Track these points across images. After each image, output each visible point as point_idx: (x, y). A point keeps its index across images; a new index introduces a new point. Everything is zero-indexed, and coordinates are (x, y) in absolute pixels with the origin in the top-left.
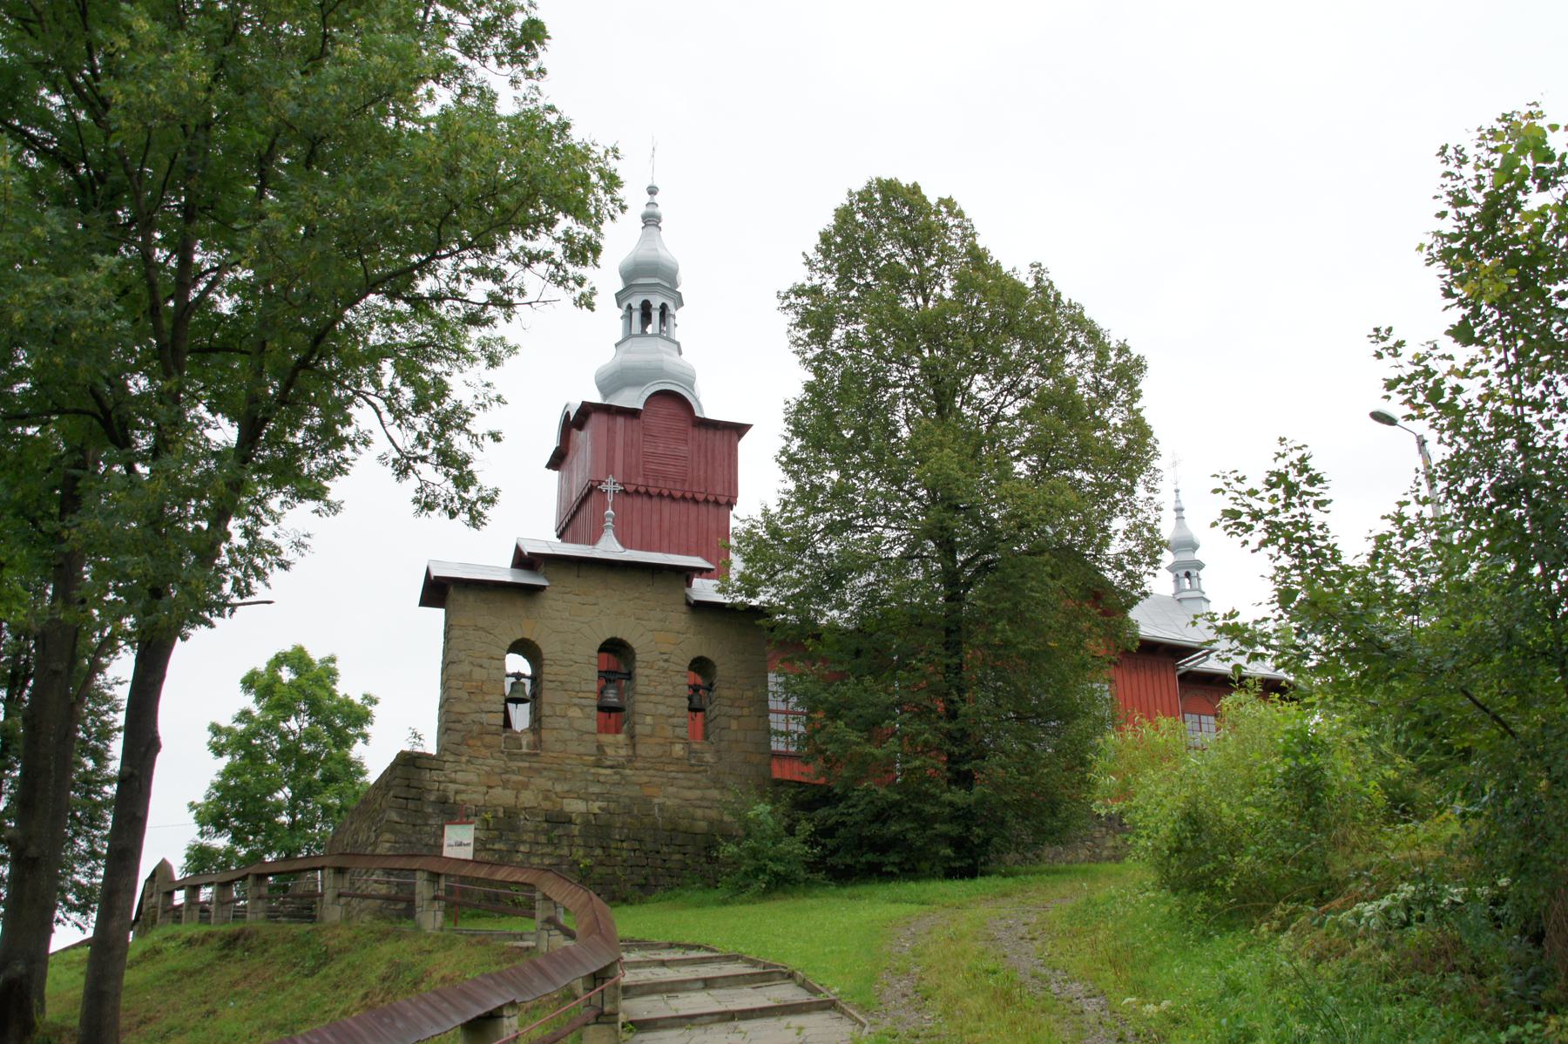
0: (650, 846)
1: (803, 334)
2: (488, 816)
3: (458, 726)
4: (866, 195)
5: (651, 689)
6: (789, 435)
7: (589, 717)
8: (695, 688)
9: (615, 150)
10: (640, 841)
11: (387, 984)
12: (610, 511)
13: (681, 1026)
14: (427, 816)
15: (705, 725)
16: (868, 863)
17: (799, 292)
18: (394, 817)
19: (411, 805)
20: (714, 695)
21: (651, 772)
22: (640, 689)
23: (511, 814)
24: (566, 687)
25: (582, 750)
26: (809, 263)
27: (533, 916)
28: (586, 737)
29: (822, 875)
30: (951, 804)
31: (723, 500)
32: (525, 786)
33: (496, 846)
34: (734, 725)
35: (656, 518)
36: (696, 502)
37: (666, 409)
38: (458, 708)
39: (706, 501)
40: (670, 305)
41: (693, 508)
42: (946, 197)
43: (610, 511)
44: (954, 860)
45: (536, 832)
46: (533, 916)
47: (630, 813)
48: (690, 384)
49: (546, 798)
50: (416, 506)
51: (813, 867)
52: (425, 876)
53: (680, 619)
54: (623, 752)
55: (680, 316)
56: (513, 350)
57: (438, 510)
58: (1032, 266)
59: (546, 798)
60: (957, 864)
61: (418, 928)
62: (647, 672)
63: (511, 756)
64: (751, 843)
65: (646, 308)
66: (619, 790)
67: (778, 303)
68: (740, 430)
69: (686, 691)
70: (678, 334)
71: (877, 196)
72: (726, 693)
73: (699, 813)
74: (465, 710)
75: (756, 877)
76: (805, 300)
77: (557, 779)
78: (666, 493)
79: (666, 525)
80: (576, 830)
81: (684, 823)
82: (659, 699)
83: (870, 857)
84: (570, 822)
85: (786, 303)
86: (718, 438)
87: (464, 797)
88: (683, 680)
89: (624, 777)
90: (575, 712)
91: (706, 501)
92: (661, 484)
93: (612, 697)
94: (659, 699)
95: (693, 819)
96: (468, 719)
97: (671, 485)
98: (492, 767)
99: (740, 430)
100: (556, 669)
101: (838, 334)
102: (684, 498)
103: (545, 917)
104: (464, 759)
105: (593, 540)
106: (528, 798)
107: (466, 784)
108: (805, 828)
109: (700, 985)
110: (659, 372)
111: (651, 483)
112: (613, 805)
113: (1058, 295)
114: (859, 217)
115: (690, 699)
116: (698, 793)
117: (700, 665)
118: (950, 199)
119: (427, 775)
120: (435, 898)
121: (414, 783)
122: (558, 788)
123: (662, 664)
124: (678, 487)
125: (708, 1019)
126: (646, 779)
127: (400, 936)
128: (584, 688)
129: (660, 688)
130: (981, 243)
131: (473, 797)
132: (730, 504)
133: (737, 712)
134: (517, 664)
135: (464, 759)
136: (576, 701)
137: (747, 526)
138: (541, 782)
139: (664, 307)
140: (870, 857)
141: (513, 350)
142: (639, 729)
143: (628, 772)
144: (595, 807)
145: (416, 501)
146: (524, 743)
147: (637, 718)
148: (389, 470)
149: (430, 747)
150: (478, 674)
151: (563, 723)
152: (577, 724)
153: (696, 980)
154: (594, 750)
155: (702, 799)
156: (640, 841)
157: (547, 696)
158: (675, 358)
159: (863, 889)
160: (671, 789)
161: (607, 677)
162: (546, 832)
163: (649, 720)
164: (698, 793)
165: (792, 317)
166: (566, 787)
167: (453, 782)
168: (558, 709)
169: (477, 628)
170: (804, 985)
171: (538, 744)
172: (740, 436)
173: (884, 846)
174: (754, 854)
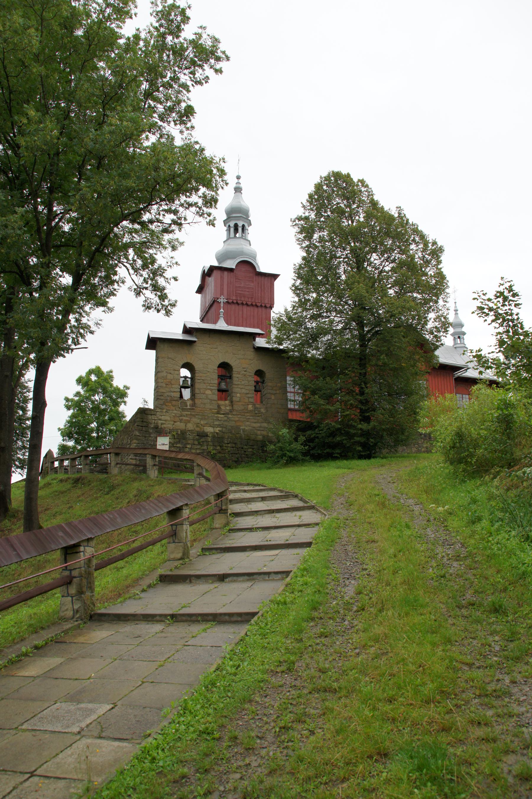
0: (239, 446)
1: (301, 236)
2: (174, 433)
3: (162, 398)
4: (327, 178)
5: (239, 383)
6: (296, 278)
7: (214, 394)
8: (257, 382)
9: (224, 159)
10: (235, 444)
11: (137, 498)
12: (222, 310)
13: (253, 515)
14: (150, 433)
15: (261, 397)
16: (327, 453)
17: (300, 219)
18: (137, 433)
19: (144, 429)
20: (265, 385)
21: (239, 416)
22: (235, 382)
23: (183, 433)
24: (206, 382)
25: (211, 407)
26: (304, 207)
27: (193, 473)
28: (213, 402)
29: (308, 458)
30: (361, 429)
31: (268, 306)
32: (189, 422)
33: (178, 445)
34: (273, 397)
35: (241, 313)
36: (257, 306)
37: (245, 268)
38: (162, 390)
39: (261, 306)
40: (246, 225)
41: (256, 309)
42: (361, 179)
43: (222, 310)
44: (362, 452)
45: (194, 440)
46: (193, 473)
47: (231, 432)
48: (255, 258)
49: (197, 426)
50: (144, 308)
51: (305, 454)
52: (150, 456)
53: (251, 354)
54: (228, 408)
55: (250, 230)
56: (182, 244)
57: (152, 309)
58: (397, 208)
59: (197, 426)
60: (363, 454)
61: (148, 477)
62: (238, 376)
63: (183, 410)
64: (280, 445)
65: (236, 227)
66: (226, 423)
67: (291, 223)
68: (275, 277)
69: (253, 384)
70: (249, 237)
71: (332, 178)
72: (270, 384)
73: (259, 432)
74: (164, 391)
75: (282, 458)
76: (302, 222)
77: (202, 419)
78: (245, 303)
79: (245, 316)
80: (209, 439)
81: (253, 437)
82: (242, 387)
83: (328, 450)
84: (207, 436)
85: (294, 223)
86: (266, 280)
87: (165, 426)
88: (252, 379)
89: (228, 418)
90: (208, 392)
91: (261, 306)
92: (243, 299)
93: (223, 386)
94: (242, 387)
95: (257, 435)
96: (166, 395)
97: (246, 299)
98: (176, 414)
99: (275, 277)
100: (201, 374)
101: (316, 236)
102: (252, 305)
103: (198, 472)
104: (164, 411)
105: (215, 322)
106: (190, 426)
107: (166, 421)
108: (302, 438)
109: (260, 499)
110: (241, 253)
111: (239, 299)
112: (224, 429)
113: (408, 220)
114: (325, 187)
115: (255, 387)
116: (259, 425)
117: (259, 373)
118: (363, 180)
119: (150, 417)
120: (154, 465)
121: (145, 420)
122: (202, 422)
123: (243, 372)
124: (250, 300)
125: (263, 512)
126: (237, 419)
127: (141, 480)
128: (212, 382)
129: (243, 382)
130: (376, 198)
131: (168, 426)
132: (271, 307)
133: (274, 392)
134: (185, 372)
135: (164, 411)
136: (209, 387)
137: (278, 316)
138: (195, 420)
139: (243, 226)
140: (328, 450)
141: (182, 244)
142: (234, 399)
143: (230, 416)
144: (217, 430)
145: (144, 306)
146: (188, 404)
147: (234, 394)
148: (133, 293)
149: (151, 406)
150: (170, 377)
151: (204, 396)
152: (210, 397)
153: (258, 498)
154: (216, 407)
155: (260, 427)
156: (235, 444)
157: (197, 386)
158: (248, 247)
159: (325, 463)
160: (247, 423)
161: (221, 378)
162: (198, 440)
163: (238, 395)
164: (259, 425)
165: (297, 229)
166: (205, 422)
167: (160, 420)
168: (202, 391)
169: (169, 358)
170: (302, 500)
171: (194, 405)
172: (275, 279)
173: (334, 446)
174: (281, 449)
